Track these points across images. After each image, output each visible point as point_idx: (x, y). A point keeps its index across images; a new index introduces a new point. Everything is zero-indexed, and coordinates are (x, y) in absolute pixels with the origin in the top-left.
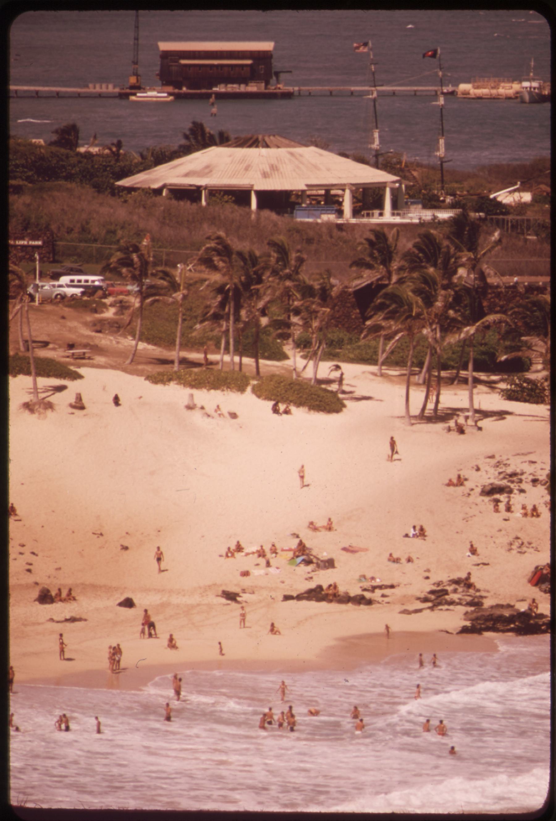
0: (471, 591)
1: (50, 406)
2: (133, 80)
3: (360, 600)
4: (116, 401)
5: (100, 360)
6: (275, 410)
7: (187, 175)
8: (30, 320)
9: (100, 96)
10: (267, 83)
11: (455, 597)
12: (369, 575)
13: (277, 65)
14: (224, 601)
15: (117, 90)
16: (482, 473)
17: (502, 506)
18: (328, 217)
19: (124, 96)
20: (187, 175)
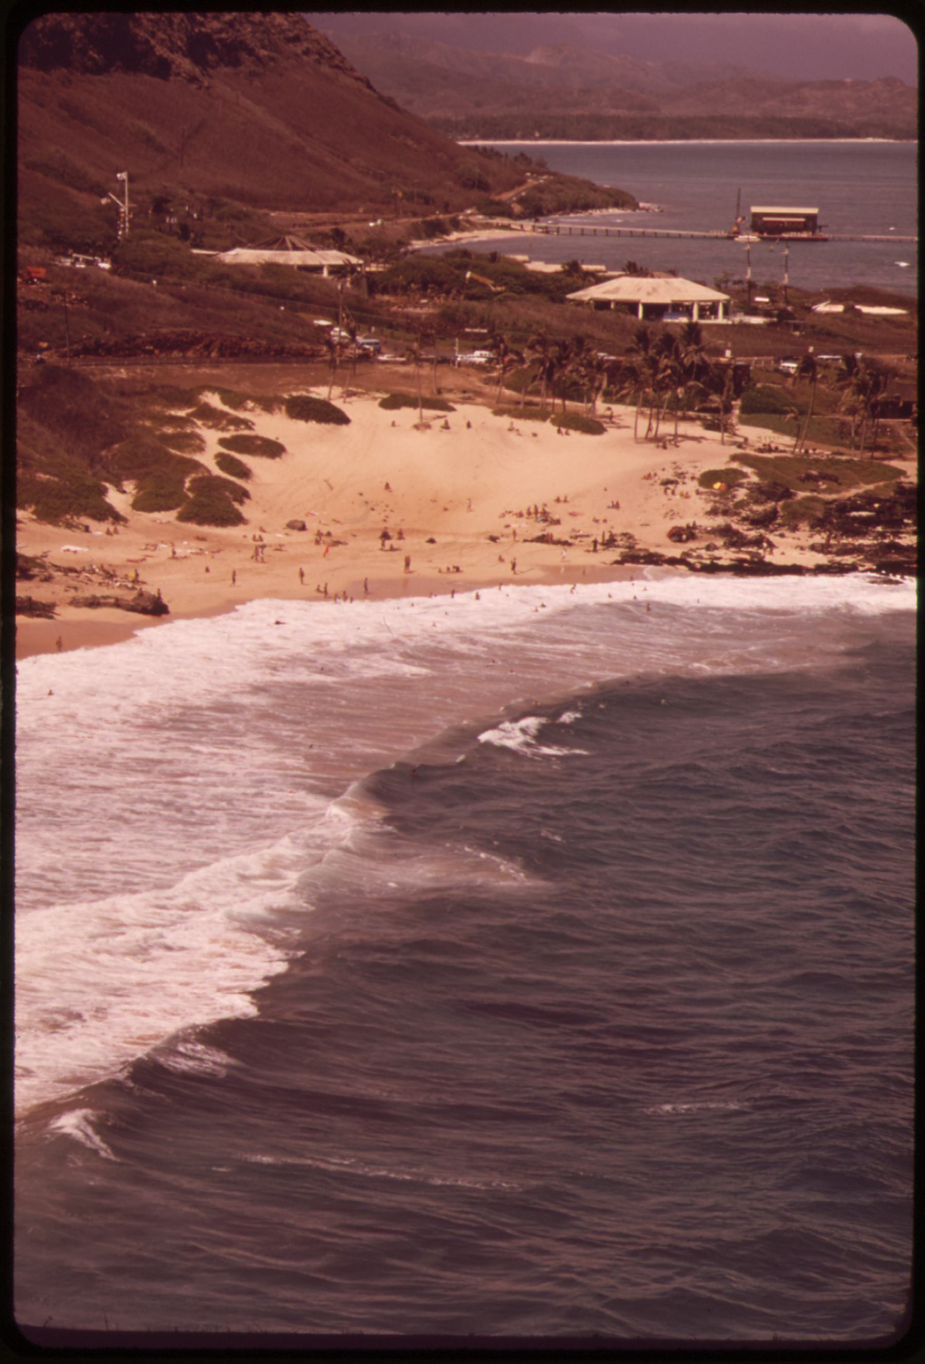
0: (631, 541)
1: (428, 426)
2: (735, 229)
3: (566, 543)
4: (469, 425)
5: (479, 400)
6: (559, 432)
7: (605, 293)
8: (138, 390)
9: (717, 238)
10: (814, 232)
11: (621, 543)
12: (577, 529)
13: (820, 222)
14: (488, 541)
15: (726, 235)
16: (665, 472)
17: (669, 492)
18: (684, 320)
19: (731, 238)
20: (605, 293)
